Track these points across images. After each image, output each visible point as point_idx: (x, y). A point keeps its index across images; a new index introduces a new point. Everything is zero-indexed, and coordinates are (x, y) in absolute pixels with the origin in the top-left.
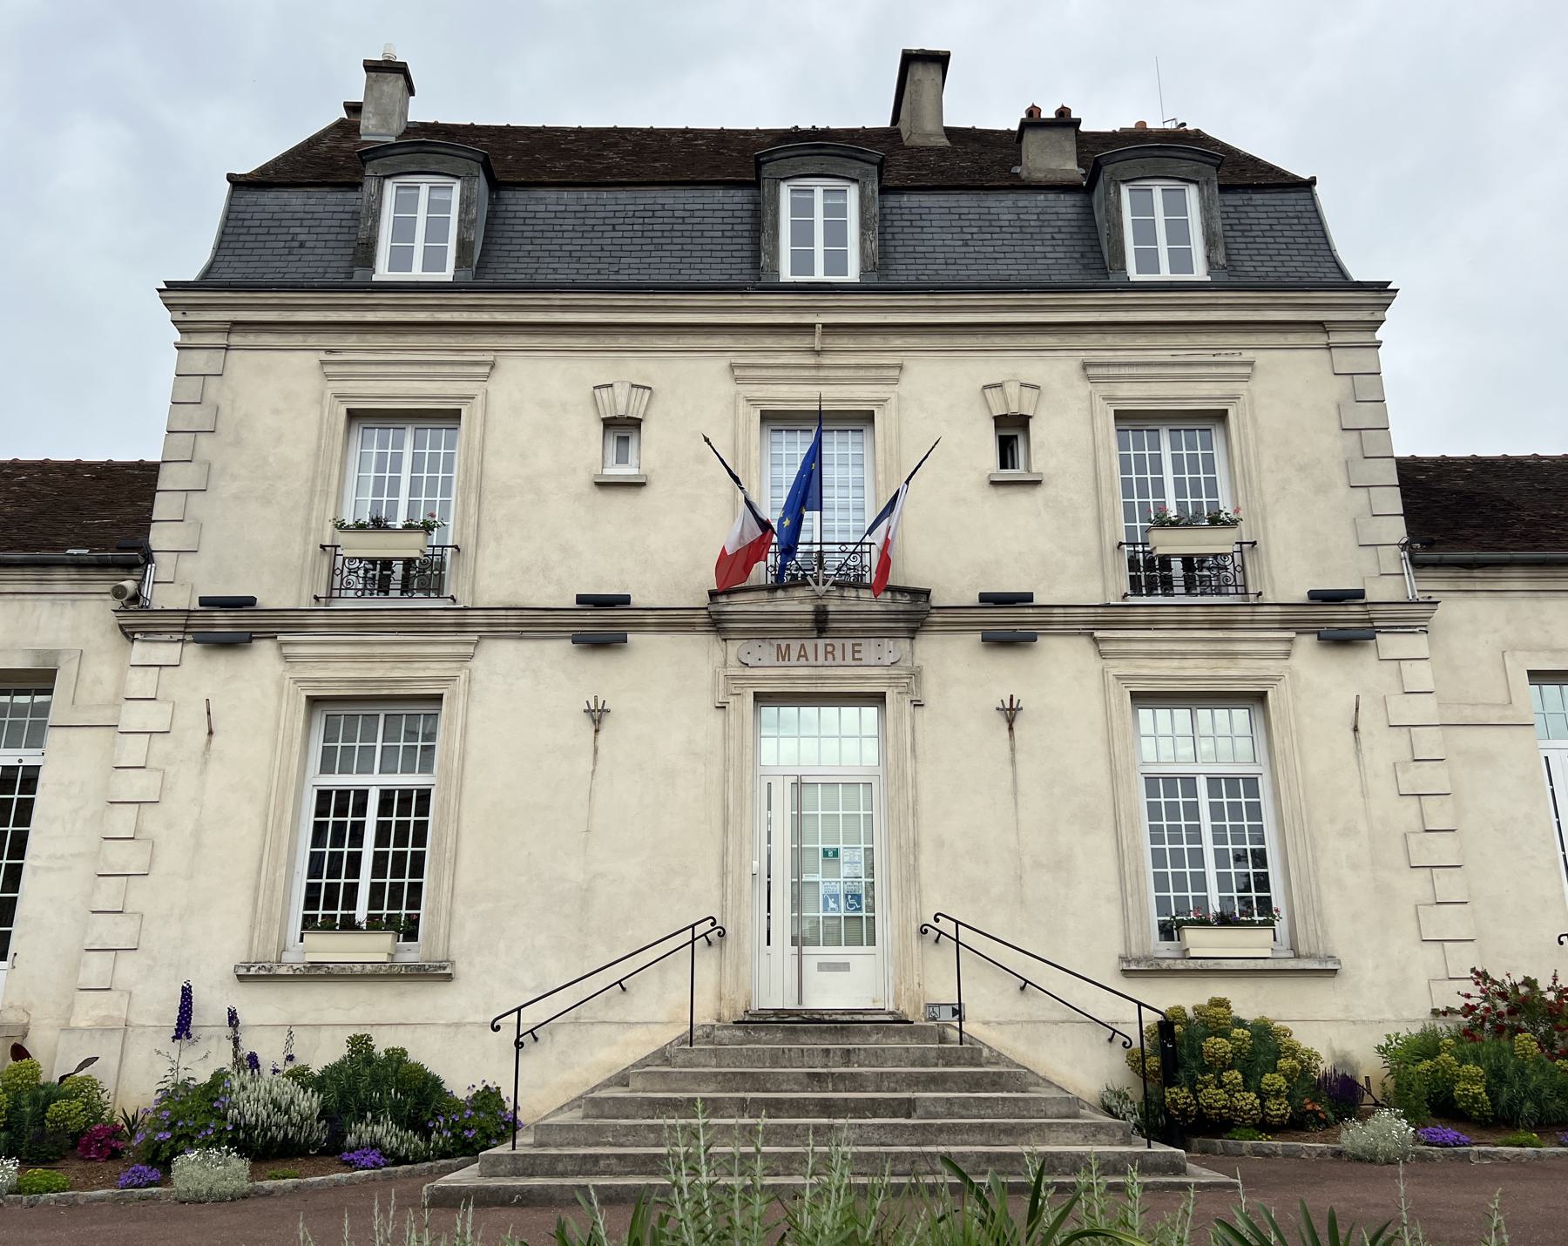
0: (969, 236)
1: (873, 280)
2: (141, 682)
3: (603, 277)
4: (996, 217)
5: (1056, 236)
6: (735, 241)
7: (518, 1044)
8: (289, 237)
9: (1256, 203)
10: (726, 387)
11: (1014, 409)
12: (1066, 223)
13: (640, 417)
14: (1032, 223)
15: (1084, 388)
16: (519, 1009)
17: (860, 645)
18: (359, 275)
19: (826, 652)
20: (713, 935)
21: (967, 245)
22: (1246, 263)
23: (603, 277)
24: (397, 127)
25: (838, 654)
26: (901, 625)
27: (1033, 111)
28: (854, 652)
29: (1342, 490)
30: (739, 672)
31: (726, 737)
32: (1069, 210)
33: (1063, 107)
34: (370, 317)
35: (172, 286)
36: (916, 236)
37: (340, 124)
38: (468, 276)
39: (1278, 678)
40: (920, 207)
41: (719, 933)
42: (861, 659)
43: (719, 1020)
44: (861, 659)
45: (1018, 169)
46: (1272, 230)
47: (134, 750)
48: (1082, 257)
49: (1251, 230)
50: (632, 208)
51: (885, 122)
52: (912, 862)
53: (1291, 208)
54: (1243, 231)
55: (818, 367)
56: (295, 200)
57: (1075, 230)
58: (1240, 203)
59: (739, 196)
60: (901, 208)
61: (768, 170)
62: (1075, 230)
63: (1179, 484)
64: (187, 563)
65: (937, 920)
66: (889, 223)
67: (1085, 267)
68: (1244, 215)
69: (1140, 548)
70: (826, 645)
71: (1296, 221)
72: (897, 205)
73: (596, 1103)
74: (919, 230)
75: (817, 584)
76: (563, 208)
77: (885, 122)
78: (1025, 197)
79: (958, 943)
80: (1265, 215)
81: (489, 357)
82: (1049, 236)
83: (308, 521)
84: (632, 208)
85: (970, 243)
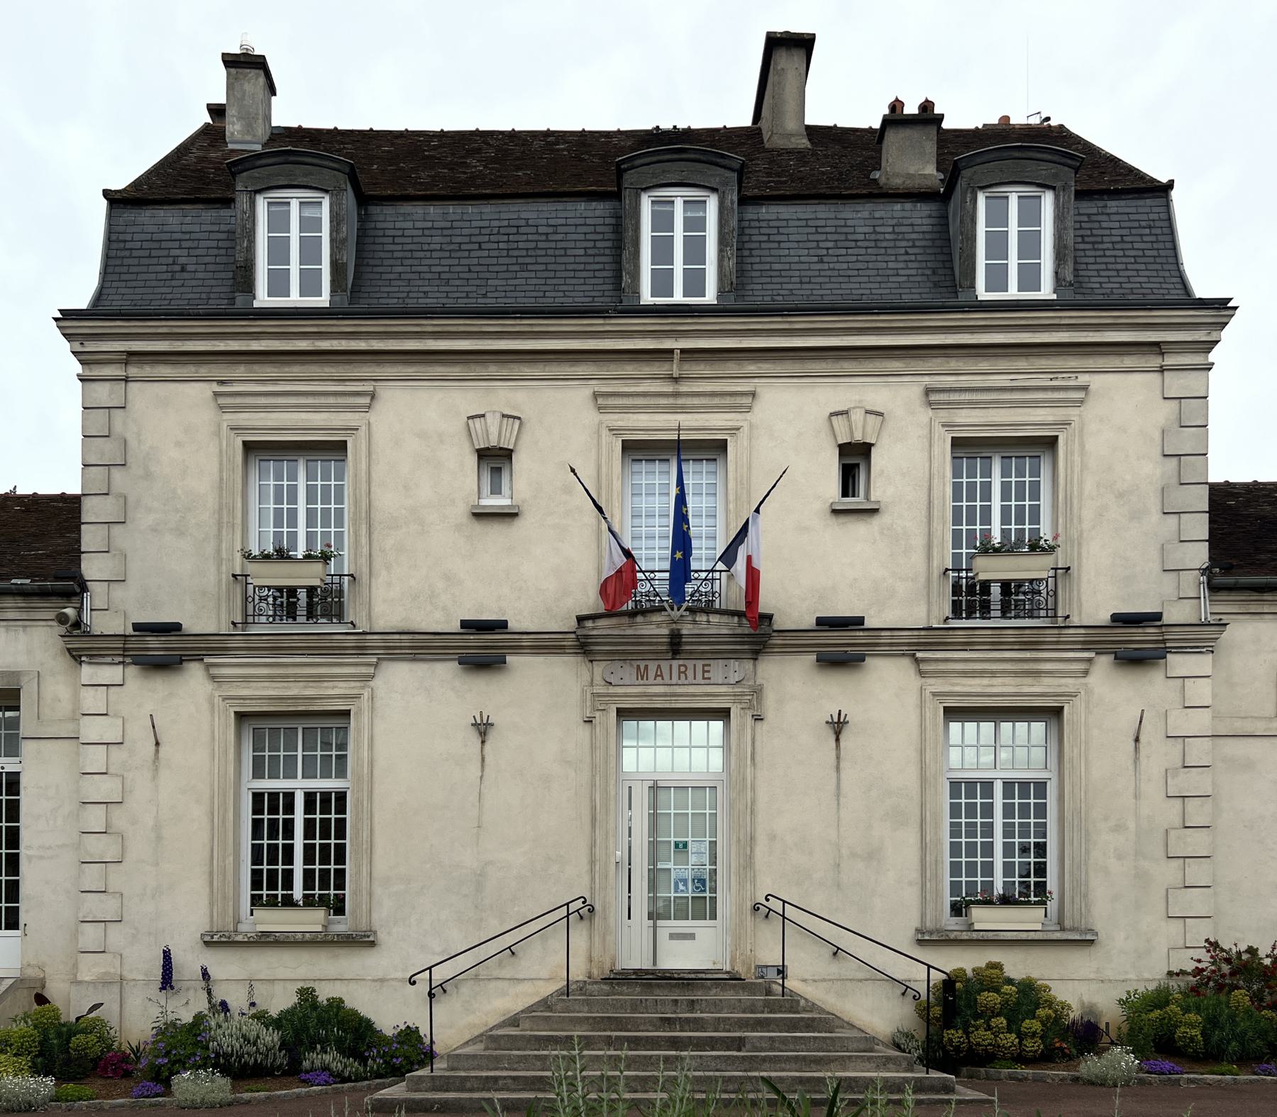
0: (825, 252)
1: (730, 302)
2: (93, 700)
4: (851, 230)
5: (910, 251)
7: (431, 995)
10: (590, 417)
11: (858, 437)
12: (921, 236)
14: (887, 236)
15: (925, 415)
16: (430, 968)
19: (680, 672)
20: (584, 911)
21: (822, 262)
25: (690, 673)
26: (746, 647)
28: (704, 671)
29: (1156, 516)
30: (602, 690)
31: (593, 748)
33: (927, 101)
35: (67, 316)
36: (773, 252)
37: (205, 131)
40: (778, 219)
41: (589, 909)
42: (709, 679)
43: (589, 977)
44: (709, 679)
45: (876, 175)
46: (1123, 241)
47: (95, 759)
48: (934, 273)
49: (1102, 242)
51: (746, 120)
52: (749, 853)
54: (1093, 243)
55: (676, 395)
56: (171, 218)
58: (1095, 210)
59: (598, 211)
60: (758, 220)
61: (629, 178)
64: (118, 592)
65: (767, 900)
68: (1096, 225)
69: (964, 574)
70: (680, 666)
71: (1147, 231)
78: (881, 207)
81: (368, 387)
82: (903, 251)
85: (825, 259)
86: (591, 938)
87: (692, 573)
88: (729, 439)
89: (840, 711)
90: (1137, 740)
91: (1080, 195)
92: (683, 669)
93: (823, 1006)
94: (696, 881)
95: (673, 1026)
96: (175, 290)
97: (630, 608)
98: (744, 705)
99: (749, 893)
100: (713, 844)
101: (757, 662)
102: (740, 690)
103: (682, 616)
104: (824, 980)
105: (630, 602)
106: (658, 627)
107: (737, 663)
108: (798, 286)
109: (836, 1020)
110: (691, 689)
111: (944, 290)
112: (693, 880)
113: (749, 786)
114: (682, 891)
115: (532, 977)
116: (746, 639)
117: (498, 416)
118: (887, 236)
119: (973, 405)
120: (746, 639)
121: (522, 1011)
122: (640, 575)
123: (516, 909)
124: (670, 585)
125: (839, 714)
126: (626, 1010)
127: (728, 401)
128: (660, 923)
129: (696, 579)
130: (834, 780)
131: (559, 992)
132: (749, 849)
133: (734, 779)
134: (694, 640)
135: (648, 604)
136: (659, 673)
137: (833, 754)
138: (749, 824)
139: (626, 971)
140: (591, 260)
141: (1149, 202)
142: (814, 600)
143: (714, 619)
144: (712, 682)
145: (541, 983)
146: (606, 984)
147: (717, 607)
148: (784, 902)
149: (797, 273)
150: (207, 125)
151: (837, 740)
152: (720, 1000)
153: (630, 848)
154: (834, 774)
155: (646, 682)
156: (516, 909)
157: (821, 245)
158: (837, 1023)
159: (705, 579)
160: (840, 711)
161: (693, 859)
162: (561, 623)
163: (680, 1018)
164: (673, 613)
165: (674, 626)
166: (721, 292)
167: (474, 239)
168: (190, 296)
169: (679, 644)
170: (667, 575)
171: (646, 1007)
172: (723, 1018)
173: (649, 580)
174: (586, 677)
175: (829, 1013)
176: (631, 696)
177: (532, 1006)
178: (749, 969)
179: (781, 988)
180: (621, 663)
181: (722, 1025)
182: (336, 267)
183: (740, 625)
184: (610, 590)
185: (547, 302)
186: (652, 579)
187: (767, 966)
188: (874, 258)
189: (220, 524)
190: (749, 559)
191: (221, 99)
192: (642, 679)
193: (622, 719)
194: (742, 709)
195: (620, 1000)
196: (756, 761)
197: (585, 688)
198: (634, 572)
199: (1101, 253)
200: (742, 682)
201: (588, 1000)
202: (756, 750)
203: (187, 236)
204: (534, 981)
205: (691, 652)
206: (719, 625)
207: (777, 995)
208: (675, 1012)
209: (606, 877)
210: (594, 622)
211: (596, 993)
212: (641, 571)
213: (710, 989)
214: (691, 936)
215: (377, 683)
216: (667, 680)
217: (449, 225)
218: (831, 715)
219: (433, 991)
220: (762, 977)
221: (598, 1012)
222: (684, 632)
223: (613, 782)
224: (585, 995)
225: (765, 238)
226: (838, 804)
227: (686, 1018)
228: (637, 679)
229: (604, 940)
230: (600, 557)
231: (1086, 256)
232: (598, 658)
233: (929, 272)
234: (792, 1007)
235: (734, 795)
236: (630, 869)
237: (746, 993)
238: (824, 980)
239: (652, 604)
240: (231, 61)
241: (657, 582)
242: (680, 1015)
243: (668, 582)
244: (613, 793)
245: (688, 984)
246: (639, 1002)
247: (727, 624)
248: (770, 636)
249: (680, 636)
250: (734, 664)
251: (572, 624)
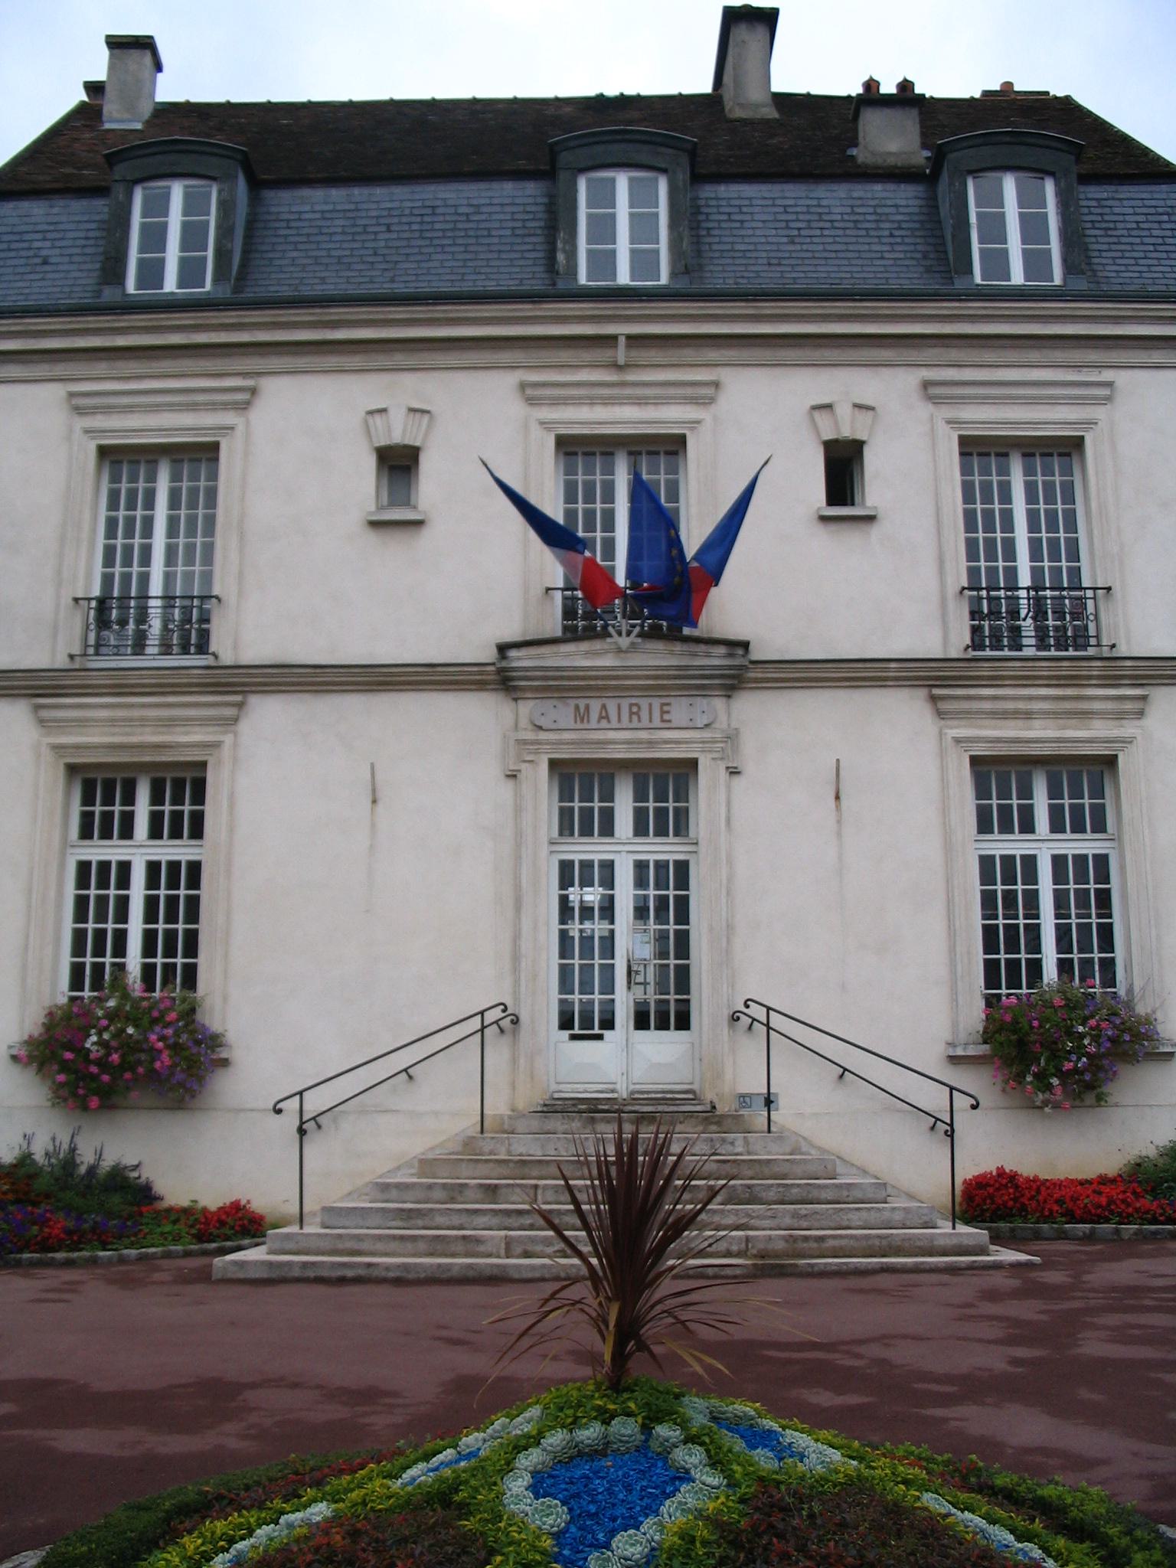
0: (796, 233)
1: (682, 285)
3: (376, 286)
6: (527, 240)
7: (302, 1132)
8: (31, 253)
9: (1121, 196)
10: (516, 408)
11: (846, 432)
13: (417, 444)
14: (869, 217)
15: (924, 410)
16: (301, 1093)
17: (668, 704)
18: (109, 295)
19: (631, 713)
20: (506, 1023)
21: (793, 243)
22: (1108, 268)
23: (376, 286)
24: (146, 111)
25: (645, 714)
27: (871, 85)
28: (663, 712)
30: (530, 736)
31: (518, 810)
32: (910, 202)
33: (905, 80)
34: (121, 341)
36: (735, 232)
37: (81, 110)
38: (225, 292)
39: (1129, 741)
40: (739, 198)
41: (512, 1021)
42: (669, 721)
43: (513, 1110)
44: (669, 721)
45: (854, 152)
48: (925, 257)
49: (1115, 229)
50: (409, 204)
51: (704, 85)
52: (724, 945)
53: (1161, 203)
54: (1106, 229)
55: (623, 384)
56: (37, 210)
57: (917, 225)
58: (1105, 195)
59: (527, 194)
62: (917, 225)
63: (1008, 525)
65: (747, 1007)
66: (703, 217)
67: (928, 270)
68: (1107, 210)
69: (984, 593)
70: (631, 705)
71: (1165, 218)
72: (713, 195)
73: (385, 1187)
74: (738, 225)
75: (620, 634)
76: (331, 207)
77: (704, 85)
78: (859, 186)
79: (769, 1028)
80: (1131, 211)
82: (887, 233)
83: (59, 572)
84: (409, 204)
85: (797, 240)
88: (688, 434)
90: (837, 797)
91: (1085, 179)
96: (35, 284)
101: (731, 700)
102: (710, 735)
108: (766, 268)
111: (937, 275)
113: (724, 856)
117: (404, 410)
118: (869, 217)
119: (984, 400)
127: (689, 391)
132: (724, 940)
140: (519, 240)
141: (1164, 187)
148: (769, 1009)
149: (764, 255)
150: (83, 104)
157: (792, 225)
166: (673, 275)
167: (382, 221)
168: (50, 290)
180: (554, 702)
182: (222, 255)
185: (466, 287)
188: (854, 240)
189: (62, 540)
191: (100, 75)
192: (582, 721)
199: (1115, 240)
203: (52, 228)
205: (756, 680)
215: (244, 726)
217: (352, 207)
219: (304, 1126)
225: (725, 217)
231: (1098, 243)
233: (919, 256)
240: (116, 44)
250: (701, 703)
251: (489, 655)
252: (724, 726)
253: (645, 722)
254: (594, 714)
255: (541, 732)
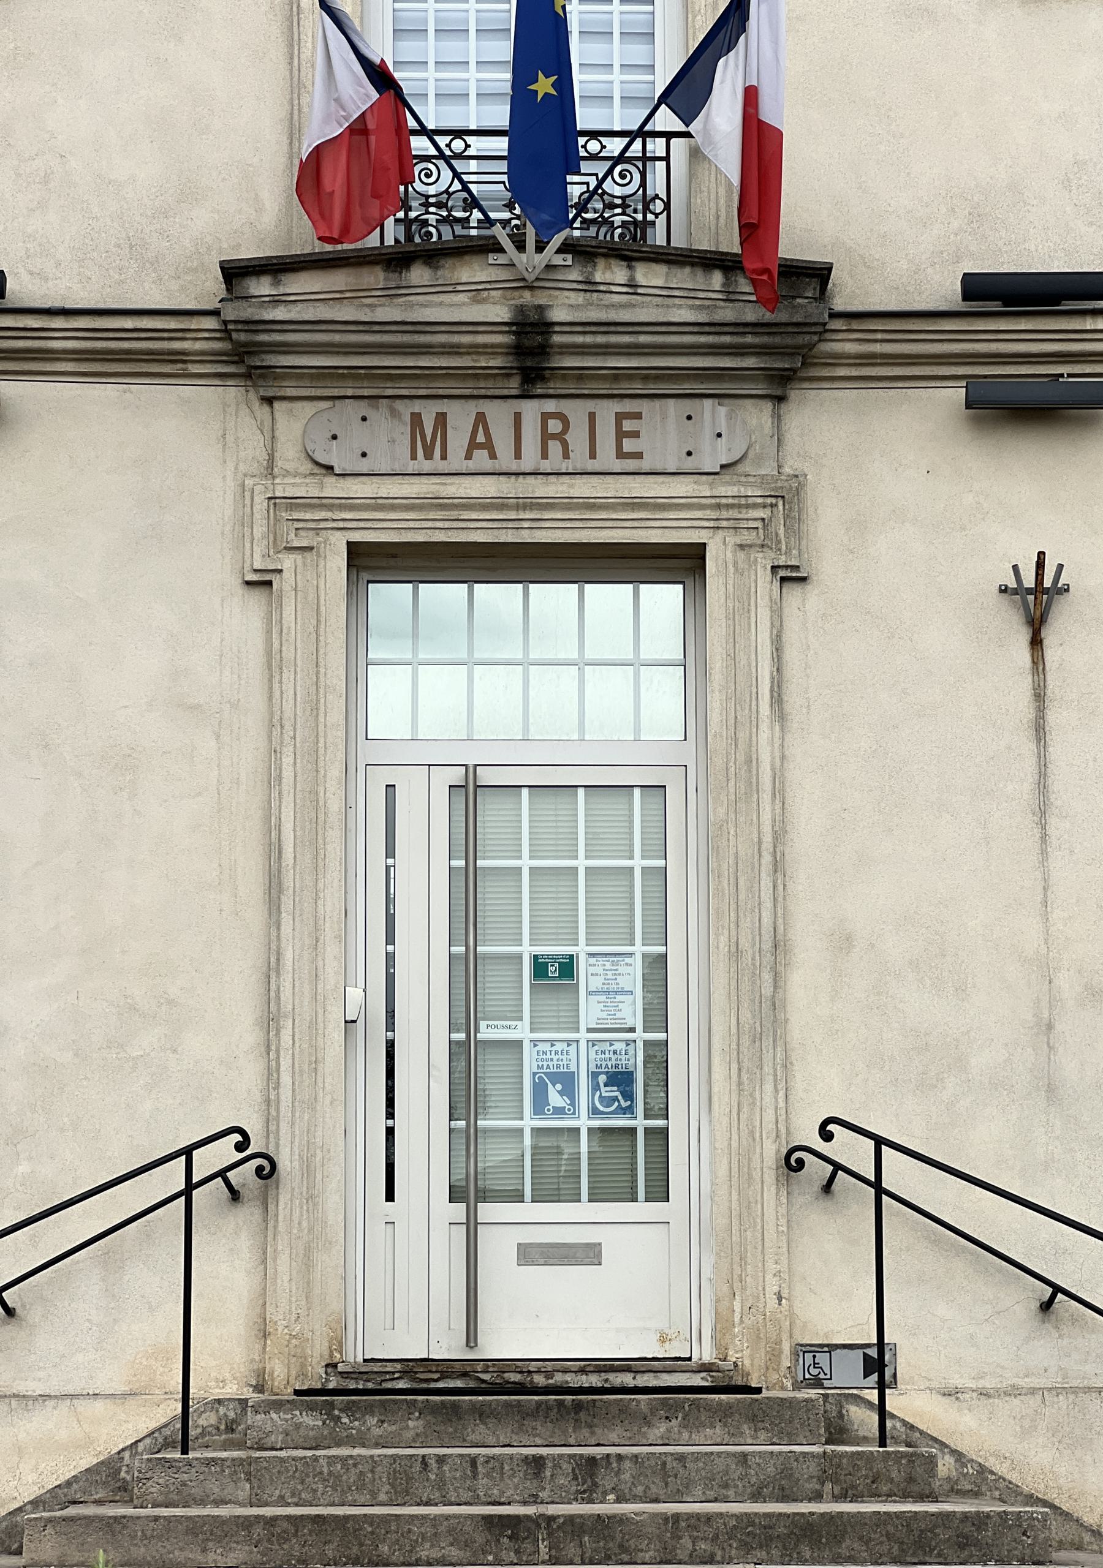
19: (546, 437)
25: (577, 438)
26: (750, 362)
28: (621, 434)
41: (259, 1170)
42: (639, 455)
43: (259, 1388)
44: (639, 455)
52: (767, 991)
65: (827, 1137)
70: (545, 417)
79: (880, 1191)
86: (264, 1262)
87: (581, 141)
89: (1041, 555)
92: (554, 426)
93: (1014, 1477)
94: (602, 1079)
95: (528, 1546)
97: (390, 241)
98: (747, 537)
99: (769, 1116)
100: (657, 965)
102: (732, 490)
103: (550, 267)
104: (1014, 1392)
105: (389, 223)
106: (476, 301)
107: (722, 411)
109: (1054, 1523)
110: (582, 488)
112: (595, 1075)
114: (559, 1111)
115: (70, 1389)
116: (749, 339)
120: (749, 339)
121: (36, 1503)
122: (420, 145)
123: (23, 1168)
124: (512, 157)
125: (1040, 565)
126: (374, 1494)
128: (487, 1211)
129: (594, 157)
130: (1029, 765)
131: (159, 1439)
132: (767, 977)
133: (719, 761)
134: (589, 339)
135: (446, 231)
136: (481, 438)
137: (1025, 684)
138: (768, 904)
139: (377, 1367)
142: (955, 224)
143: (650, 276)
144: (645, 465)
145: (99, 1407)
146: (311, 1408)
147: (661, 241)
148: (879, 1142)
151: (1036, 642)
152: (681, 1458)
153: (390, 901)
154: (1029, 748)
155: (437, 464)
156: (23, 1168)
158: (1057, 1530)
159: (621, 158)
160: (1041, 555)
161: (591, 1011)
162: (174, 285)
163: (551, 1519)
164: (521, 259)
165: (527, 297)
169: (544, 350)
170: (501, 145)
171: (441, 1484)
172: (690, 1516)
173: (447, 160)
174: (254, 447)
175: (1031, 1499)
176: (393, 508)
177: (69, 1483)
178: (775, 1355)
179: (876, 1417)
180: (363, 408)
181: (686, 1542)
183: (730, 296)
184: (334, 179)
186: (459, 156)
187: (832, 1348)
190: (751, 96)
192: (429, 456)
193: (365, 576)
194: (742, 547)
195: (357, 1461)
196: (788, 708)
197: (249, 482)
198: (402, 134)
200: (740, 468)
201: (250, 1461)
202: (788, 673)
204: (80, 1404)
205: (581, 375)
206: (667, 294)
207: (865, 1440)
208: (534, 1500)
209: (315, 1064)
210: (276, 283)
211: (277, 1439)
212: (423, 131)
213: (647, 1421)
214: (590, 1254)
216: (506, 460)
218: (1015, 568)
220: (817, 1383)
221: (282, 1502)
222: (558, 315)
223: (335, 772)
224: (241, 1445)
226: (1044, 838)
227: (571, 1519)
228: (414, 457)
229: (308, 1263)
230: (296, 87)
232: (290, 392)
234: (911, 1480)
235: (721, 811)
236: (390, 1046)
237: (763, 1436)
238: (1014, 1392)
239: (458, 230)
241: (473, 165)
242: (552, 1510)
243: (503, 166)
244: (335, 805)
245: (578, 1407)
246: (418, 1467)
247: (689, 295)
248: (823, 332)
249: (547, 327)
252: (768, 469)
253: (579, 458)
254: (457, 441)
255: (331, 480)
